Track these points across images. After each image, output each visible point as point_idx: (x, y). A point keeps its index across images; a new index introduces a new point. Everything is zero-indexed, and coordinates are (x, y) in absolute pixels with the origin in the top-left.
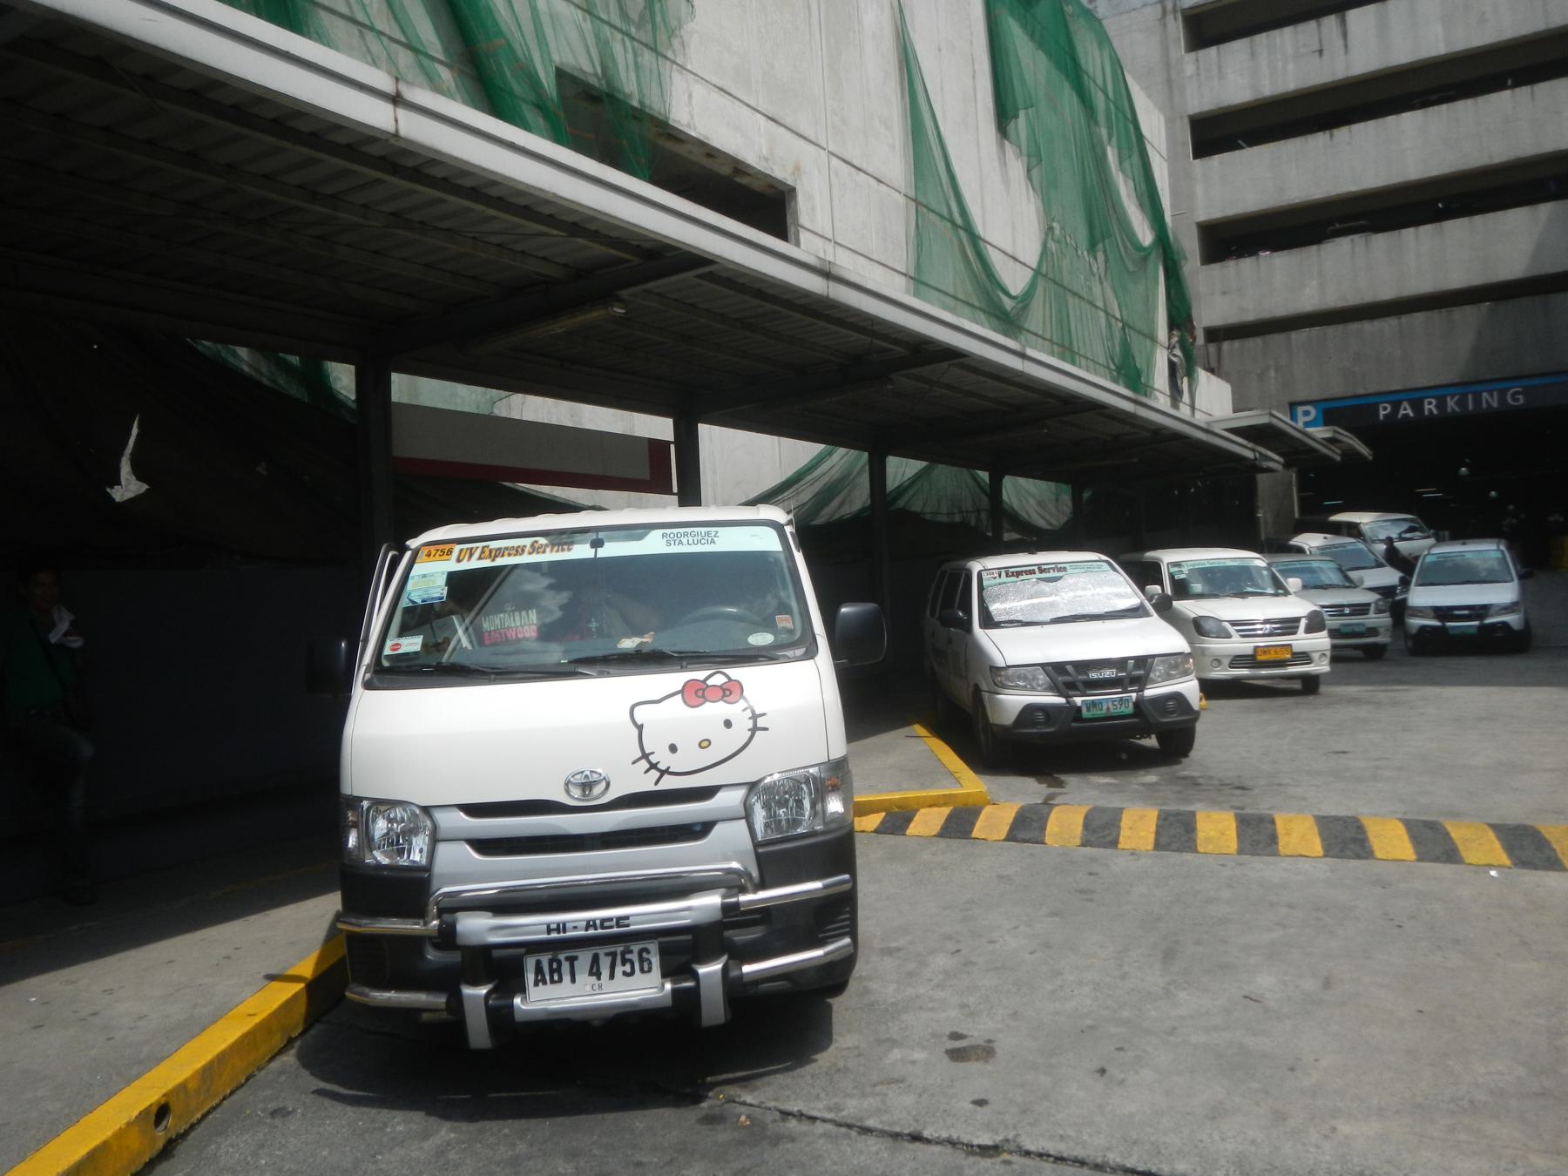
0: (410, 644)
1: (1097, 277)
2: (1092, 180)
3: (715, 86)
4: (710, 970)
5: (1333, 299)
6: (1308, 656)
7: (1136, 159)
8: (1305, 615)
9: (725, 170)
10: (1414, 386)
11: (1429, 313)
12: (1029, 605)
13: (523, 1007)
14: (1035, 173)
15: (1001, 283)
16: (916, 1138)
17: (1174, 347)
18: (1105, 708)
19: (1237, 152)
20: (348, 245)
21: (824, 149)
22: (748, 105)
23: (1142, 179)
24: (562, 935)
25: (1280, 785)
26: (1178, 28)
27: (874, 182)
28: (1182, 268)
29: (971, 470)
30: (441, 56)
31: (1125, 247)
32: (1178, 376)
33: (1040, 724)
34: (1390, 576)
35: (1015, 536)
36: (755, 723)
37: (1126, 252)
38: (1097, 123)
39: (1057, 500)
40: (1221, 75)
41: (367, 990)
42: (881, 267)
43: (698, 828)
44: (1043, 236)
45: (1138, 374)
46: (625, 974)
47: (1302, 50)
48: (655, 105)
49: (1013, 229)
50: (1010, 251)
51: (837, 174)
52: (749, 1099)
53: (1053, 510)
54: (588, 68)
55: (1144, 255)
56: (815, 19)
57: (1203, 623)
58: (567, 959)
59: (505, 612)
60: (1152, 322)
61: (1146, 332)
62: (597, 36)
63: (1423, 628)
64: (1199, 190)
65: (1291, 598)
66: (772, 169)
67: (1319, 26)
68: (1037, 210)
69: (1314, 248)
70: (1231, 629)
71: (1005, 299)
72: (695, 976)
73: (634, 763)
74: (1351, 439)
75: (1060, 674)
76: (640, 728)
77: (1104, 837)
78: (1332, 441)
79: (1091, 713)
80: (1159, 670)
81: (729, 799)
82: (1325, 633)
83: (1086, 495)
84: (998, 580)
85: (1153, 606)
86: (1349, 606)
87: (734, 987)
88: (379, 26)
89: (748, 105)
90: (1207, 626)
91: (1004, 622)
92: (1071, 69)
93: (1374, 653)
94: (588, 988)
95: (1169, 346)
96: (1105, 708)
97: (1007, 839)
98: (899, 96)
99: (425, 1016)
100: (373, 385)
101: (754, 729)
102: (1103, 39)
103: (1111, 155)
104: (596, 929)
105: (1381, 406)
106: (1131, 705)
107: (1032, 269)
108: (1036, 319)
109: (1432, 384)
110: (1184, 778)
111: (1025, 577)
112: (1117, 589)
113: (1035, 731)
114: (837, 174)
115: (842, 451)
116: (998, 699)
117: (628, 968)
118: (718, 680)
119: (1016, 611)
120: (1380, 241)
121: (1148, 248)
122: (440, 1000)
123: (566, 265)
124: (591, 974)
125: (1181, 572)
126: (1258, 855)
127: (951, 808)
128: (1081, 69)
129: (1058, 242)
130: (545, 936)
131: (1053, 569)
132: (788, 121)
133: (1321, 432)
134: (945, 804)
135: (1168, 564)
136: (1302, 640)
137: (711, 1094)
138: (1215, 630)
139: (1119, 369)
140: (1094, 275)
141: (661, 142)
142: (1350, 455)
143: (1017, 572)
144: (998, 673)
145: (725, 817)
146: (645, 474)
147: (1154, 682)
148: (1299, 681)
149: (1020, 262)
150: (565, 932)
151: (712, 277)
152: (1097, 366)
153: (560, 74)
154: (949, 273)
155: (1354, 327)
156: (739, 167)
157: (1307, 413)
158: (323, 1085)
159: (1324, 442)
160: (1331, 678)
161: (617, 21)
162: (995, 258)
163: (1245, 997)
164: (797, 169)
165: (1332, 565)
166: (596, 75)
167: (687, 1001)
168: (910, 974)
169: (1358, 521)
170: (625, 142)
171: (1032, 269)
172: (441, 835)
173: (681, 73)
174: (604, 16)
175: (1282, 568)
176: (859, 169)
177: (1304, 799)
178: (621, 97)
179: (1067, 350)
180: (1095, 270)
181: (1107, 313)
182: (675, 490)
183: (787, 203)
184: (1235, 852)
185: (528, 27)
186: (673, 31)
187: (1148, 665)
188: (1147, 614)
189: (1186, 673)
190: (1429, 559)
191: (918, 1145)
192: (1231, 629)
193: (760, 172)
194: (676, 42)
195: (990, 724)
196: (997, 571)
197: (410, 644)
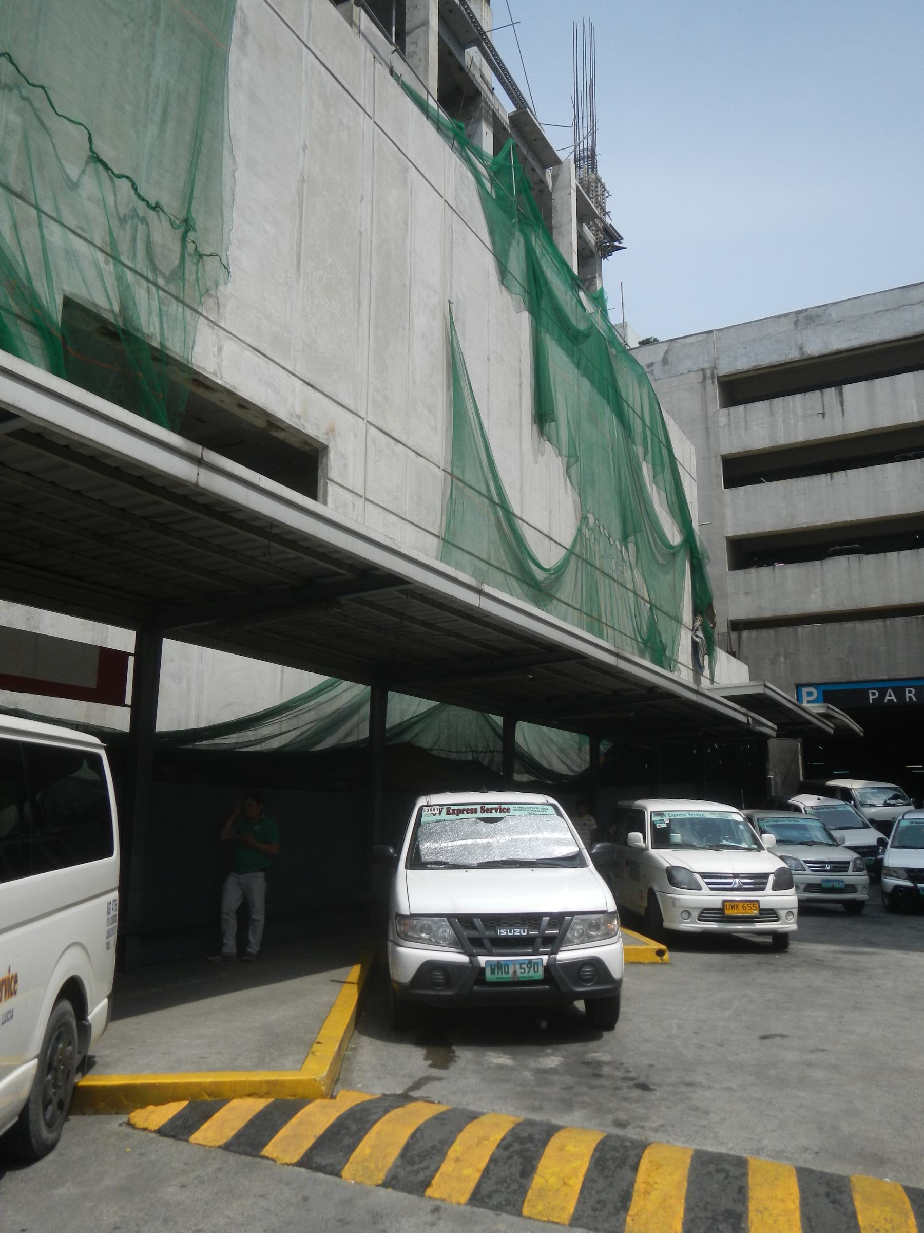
3: (249, 346)
5: (832, 604)
6: (775, 913)
7: (668, 474)
8: (773, 871)
9: (260, 423)
10: (897, 677)
11: (908, 618)
12: (461, 846)
14: (574, 470)
15: (533, 556)
17: (697, 630)
18: (511, 971)
21: (363, 419)
23: (673, 491)
25: (690, 1084)
26: (715, 389)
28: (705, 567)
29: (486, 714)
33: (438, 985)
34: (870, 837)
35: (525, 778)
37: (656, 547)
39: (580, 750)
42: (413, 527)
44: (579, 523)
47: (809, 412)
48: (175, 348)
49: (550, 512)
50: (546, 531)
55: (673, 552)
57: (675, 873)
60: (678, 606)
61: (672, 613)
63: (897, 887)
64: (728, 512)
65: (764, 853)
67: (822, 395)
69: (818, 563)
70: (702, 882)
74: (842, 715)
75: (467, 928)
79: (496, 976)
82: (792, 891)
83: (604, 747)
85: (591, 855)
86: (830, 862)
90: (679, 876)
91: (431, 863)
93: (853, 909)
96: (511, 971)
97: (300, 1164)
103: (646, 471)
105: (870, 691)
106: (541, 970)
108: (567, 590)
109: (911, 676)
111: (465, 815)
113: (432, 992)
119: (447, 851)
120: (870, 560)
121: (677, 546)
125: (663, 821)
127: (271, 1100)
128: (622, 398)
131: (496, 810)
132: (326, 389)
134: (267, 1095)
135: (651, 813)
136: (769, 897)
139: (645, 642)
142: (842, 730)
143: (458, 810)
146: (91, 682)
147: (571, 942)
148: (771, 936)
149: (556, 542)
153: (68, 303)
155: (848, 625)
156: (272, 422)
157: (810, 694)
159: (818, 716)
160: (799, 936)
162: (531, 538)
164: (331, 430)
166: (112, 311)
169: (850, 787)
173: (213, 328)
179: (595, 623)
180: (626, 557)
181: (634, 593)
182: (128, 700)
183: (320, 458)
184: (567, 1222)
186: (208, 290)
188: (583, 864)
189: (609, 935)
190: (904, 824)
192: (702, 882)
193: (290, 427)
196: (438, 807)
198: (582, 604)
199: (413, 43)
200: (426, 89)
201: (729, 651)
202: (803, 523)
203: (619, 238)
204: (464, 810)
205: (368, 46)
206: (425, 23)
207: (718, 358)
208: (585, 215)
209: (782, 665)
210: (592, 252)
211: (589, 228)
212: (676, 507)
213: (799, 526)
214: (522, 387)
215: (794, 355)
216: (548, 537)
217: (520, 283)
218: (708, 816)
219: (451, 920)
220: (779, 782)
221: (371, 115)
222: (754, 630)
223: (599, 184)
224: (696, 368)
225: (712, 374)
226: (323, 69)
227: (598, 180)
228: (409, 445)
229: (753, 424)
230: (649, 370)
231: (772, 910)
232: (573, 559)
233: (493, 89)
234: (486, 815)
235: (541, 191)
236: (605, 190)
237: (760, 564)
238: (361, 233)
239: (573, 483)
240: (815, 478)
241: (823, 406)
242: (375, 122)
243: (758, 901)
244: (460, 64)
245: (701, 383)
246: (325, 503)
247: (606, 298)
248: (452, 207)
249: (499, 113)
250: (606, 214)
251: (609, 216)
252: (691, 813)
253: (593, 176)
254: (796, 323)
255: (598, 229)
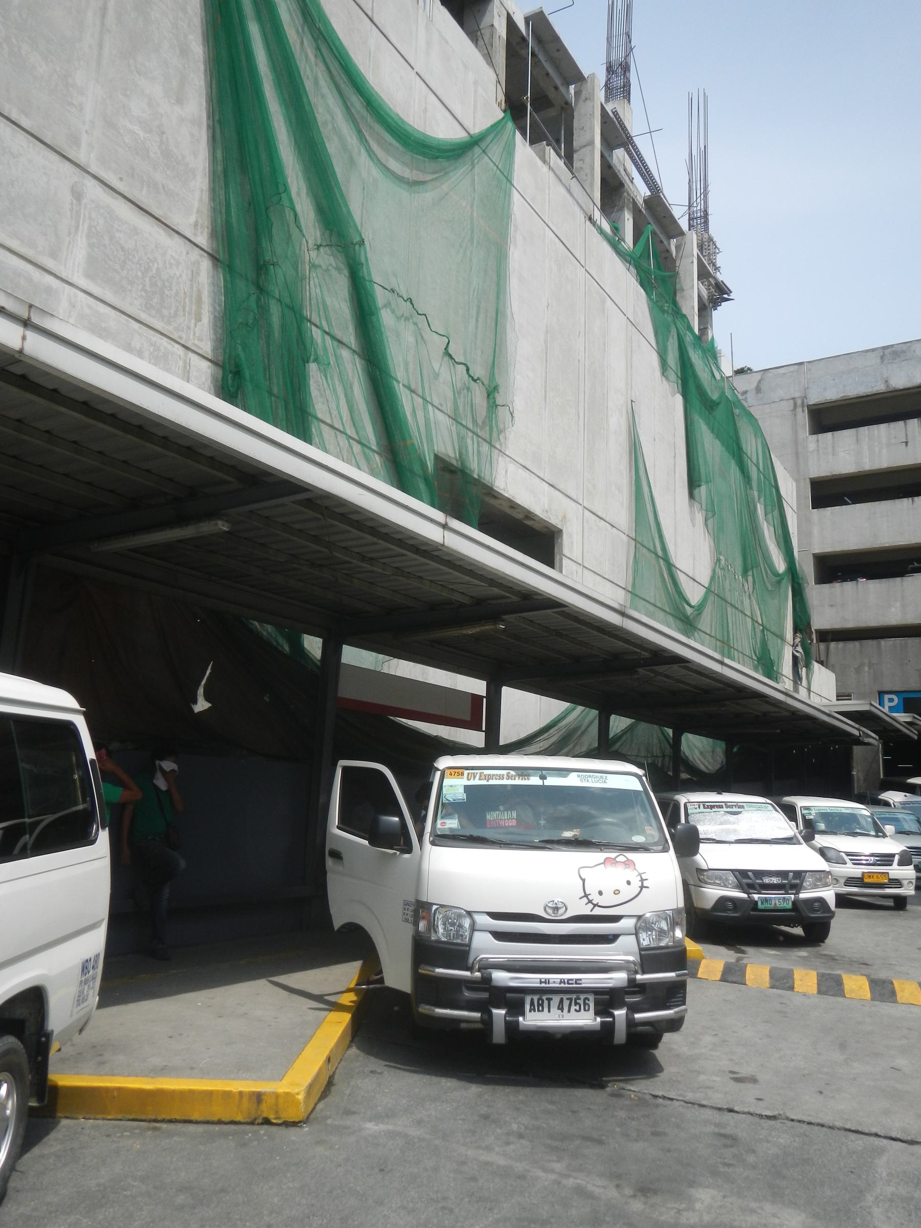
0: (451, 823)
1: (747, 594)
2: (746, 527)
4: (620, 1013)
7: (776, 513)
9: (520, 516)
13: (525, 1023)
14: (710, 522)
16: (731, 1111)
17: (797, 645)
18: (773, 903)
19: (844, 506)
20: (358, 579)
22: (539, 477)
23: (780, 525)
24: (547, 985)
26: (805, 417)
27: (609, 527)
30: (374, 448)
31: (767, 573)
32: (800, 667)
33: (730, 910)
36: (642, 884)
37: (767, 577)
38: (751, 488)
39: (713, 752)
40: (834, 454)
41: (433, 1008)
42: (610, 583)
43: (611, 937)
45: (772, 664)
46: (576, 1010)
48: (487, 479)
50: (691, 575)
51: (587, 522)
52: (632, 1088)
53: (711, 761)
54: (451, 454)
55: (779, 578)
56: (581, 423)
57: (826, 851)
58: (547, 999)
59: (498, 810)
60: (782, 627)
61: (778, 633)
62: (458, 434)
64: (816, 531)
66: (550, 518)
67: (906, 425)
68: (710, 547)
69: (898, 579)
70: (846, 858)
71: (687, 607)
72: (613, 1016)
73: (580, 899)
75: (744, 878)
76: (584, 881)
77: (784, 984)
78: (910, 724)
80: (809, 881)
81: (627, 924)
82: (912, 867)
84: (698, 810)
87: (631, 1023)
88: (349, 433)
89: (539, 477)
92: (737, 452)
94: (557, 1016)
95: (794, 644)
96: (773, 903)
98: (628, 470)
99: (463, 1025)
100: (332, 651)
101: (642, 887)
102: (758, 431)
104: (565, 984)
106: (790, 903)
107: (706, 588)
108: (706, 622)
110: (826, 955)
111: (716, 809)
112: (781, 826)
114: (587, 522)
115: (580, 708)
116: (703, 892)
117: (577, 1007)
118: (621, 859)
121: (782, 575)
122: (477, 1015)
123: (472, 597)
124: (559, 1009)
126: (884, 1002)
129: (723, 569)
130: (539, 985)
131: (735, 806)
132: (561, 487)
133: (903, 717)
135: (801, 807)
136: (896, 871)
137: (609, 1085)
138: (834, 858)
139: (759, 660)
140: (745, 592)
141: (487, 499)
143: (711, 806)
144: (702, 873)
145: (625, 933)
146: (467, 717)
150: (549, 983)
151: (562, 614)
152: (745, 656)
153: (437, 457)
154: (652, 590)
156: (529, 515)
157: (891, 700)
158: (387, 1063)
161: (470, 426)
162: (682, 578)
163: (892, 1068)
165: (912, 817)
167: (608, 1029)
168: (693, 1043)
170: (468, 501)
171: (706, 588)
172: (477, 927)
174: (464, 423)
175: (477, 782)
176: (601, 518)
177: (908, 974)
178: (468, 471)
180: (746, 589)
185: (423, 430)
187: (802, 878)
191: (732, 1114)
192: (846, 858)
193: (542, 519)
194: (501, 437)
195: (695, 908)
197: (451, 823)
198: (711, 631)
199: (581, 160)
200: (592, 201)
201: (818, 659)
202: (885, 543)
203: (729, 292)
204: (714, 806)
205: (582, 212)
206: (591, 143)
207: (808, 388)
208: (704, 274)
209: (866, 674)
210: (705, 305)
211: (702, 284)
212: (781, 540)
213: (881, 546)
214: (676, 458)
215: (880, 387)
216: (693, 579)
217: (514, 187)
218: (844, 811)
219: (734, 873)
220: (862, 778)
221: (584, 265)
222: (841, 642)
223: (712, 243)
224: (788, 397)
225: (803, 403)
226: (557, 239)
227: (711, 239)
228: (607, 520)
229: (840, 450)
230: (743, 397)
231: (897, 880)
232: (711, 598)
233: (633, 179)
234: (729, 810)
235: (666, 258)
236: (716, 247)
237: (844, 579)
238: (579, 361)
239: (709, 531)
240: (898, 501)
241: (907, 435)
242: (586, 270)
243: (888, 873)
244: (609, 163)
245: (793, 410)
246: (561, 572)
247: (716, 346)
248: (631, 322)
249: (637, 199)
250: (717, 269)
251: (719, 271)
252: (831, 808)
253: (706, 236)
254: (882, 358)
255: (710, 284)
